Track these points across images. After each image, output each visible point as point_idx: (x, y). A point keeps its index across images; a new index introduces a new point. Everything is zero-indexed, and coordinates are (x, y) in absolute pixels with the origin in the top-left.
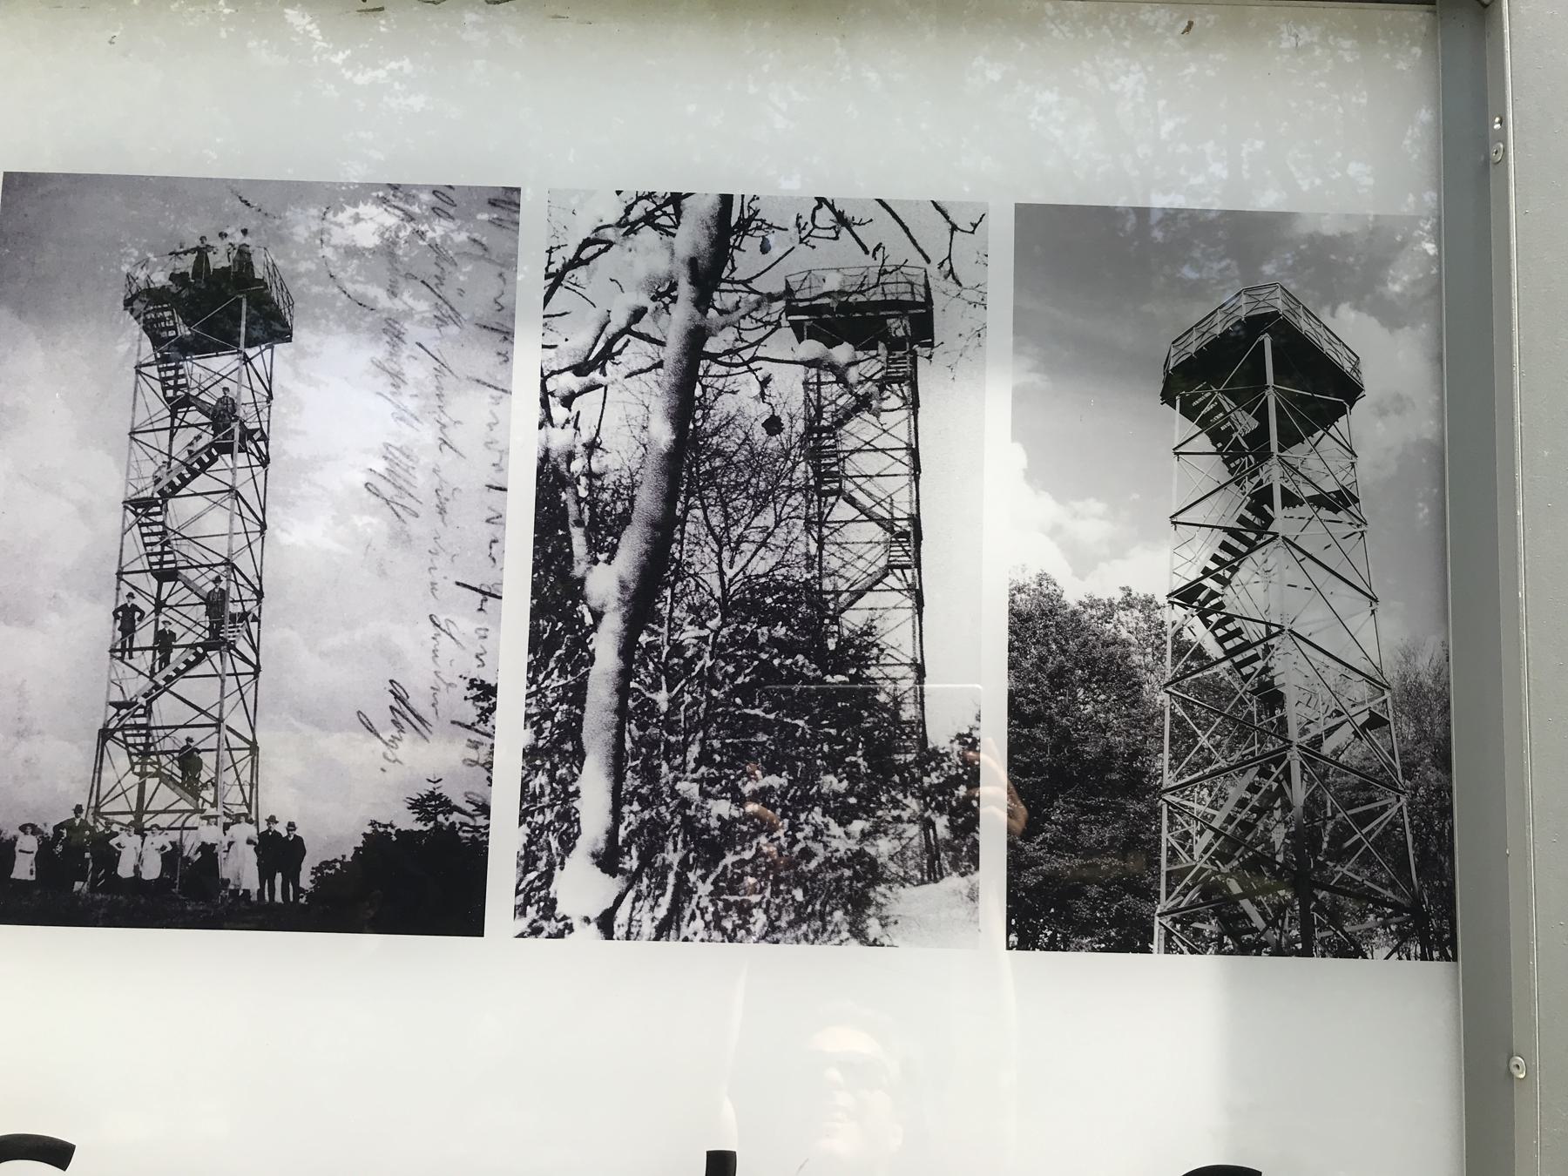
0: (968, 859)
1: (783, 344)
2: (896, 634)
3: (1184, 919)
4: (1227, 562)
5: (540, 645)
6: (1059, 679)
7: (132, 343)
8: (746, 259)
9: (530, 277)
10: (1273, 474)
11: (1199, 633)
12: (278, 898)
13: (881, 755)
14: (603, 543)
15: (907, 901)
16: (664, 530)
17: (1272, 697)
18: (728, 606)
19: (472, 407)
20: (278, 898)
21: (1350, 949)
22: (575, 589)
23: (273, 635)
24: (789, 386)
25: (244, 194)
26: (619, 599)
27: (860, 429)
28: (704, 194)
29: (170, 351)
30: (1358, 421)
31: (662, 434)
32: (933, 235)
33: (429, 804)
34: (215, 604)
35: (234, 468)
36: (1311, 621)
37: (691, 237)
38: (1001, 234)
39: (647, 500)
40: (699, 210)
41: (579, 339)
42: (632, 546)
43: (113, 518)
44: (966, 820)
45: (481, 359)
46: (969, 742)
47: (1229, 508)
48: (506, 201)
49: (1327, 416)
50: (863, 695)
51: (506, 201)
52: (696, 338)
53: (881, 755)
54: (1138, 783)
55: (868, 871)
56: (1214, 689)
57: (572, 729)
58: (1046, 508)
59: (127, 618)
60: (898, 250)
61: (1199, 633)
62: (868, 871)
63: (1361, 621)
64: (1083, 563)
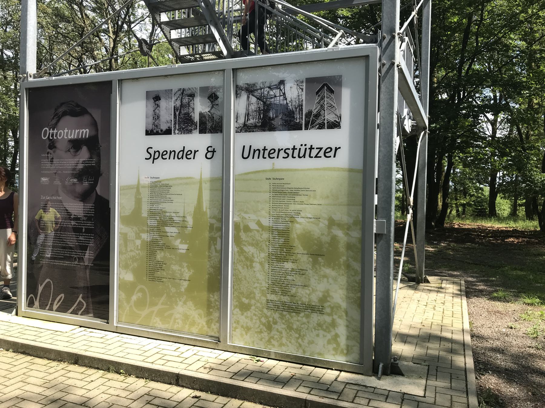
0: (197, 129)
1: (187, 97)
2: (193, 115)
3: (208, 131)
4: (211, 109)
5: (174, 117)
6: (202, 117)
7: (152, 101)
8: (185, 92)
9: (173, 95)
10: (214, 103)
11: (209, 114)
12: (94, 212)
13: (192, 123)
14: (177, 110)
15: (193, 131)
16: (180, 110)
17: (213, 118)
18: (184, 114)
19: (170, 103)
20: (94, 212)
21: (217, 133)
22: (176, 114)
23: (161, 118)
24: (187, 100)
25: (158, 91)
26: (352, 302)
27: (191, 102)
28: (182, 88)
29: (155, 101)
30: (219, 99)
31: (180, 104)
32: (195, 89)
33: (169, 127)
34: (158, 116)
35: (158, 108)
36: (216, 113)
37: (182, 91)
38: (199, 88)
39: (179, 108)
40: (182, 89)
41: (176, 98)
42: (179, 111)
43: (153, 111)
44: (197, 126)
45: (170, 100)
46: (197, 122)
47: (211, 106)
48: (172, 90)
49: (217, 99)
50: (191, 119)
51: (172, 90)
52: (182, 97)
53: (192, 123)
54: (206, 123)
55: (192, 130)
56: (210, 117)
57: (176, 122)
58: (201, 106)
59: (153, 117)
60: (193, 91)
61: (209, 114)
62: (192, 130)
63: (218, 112)
64: (203, 110)
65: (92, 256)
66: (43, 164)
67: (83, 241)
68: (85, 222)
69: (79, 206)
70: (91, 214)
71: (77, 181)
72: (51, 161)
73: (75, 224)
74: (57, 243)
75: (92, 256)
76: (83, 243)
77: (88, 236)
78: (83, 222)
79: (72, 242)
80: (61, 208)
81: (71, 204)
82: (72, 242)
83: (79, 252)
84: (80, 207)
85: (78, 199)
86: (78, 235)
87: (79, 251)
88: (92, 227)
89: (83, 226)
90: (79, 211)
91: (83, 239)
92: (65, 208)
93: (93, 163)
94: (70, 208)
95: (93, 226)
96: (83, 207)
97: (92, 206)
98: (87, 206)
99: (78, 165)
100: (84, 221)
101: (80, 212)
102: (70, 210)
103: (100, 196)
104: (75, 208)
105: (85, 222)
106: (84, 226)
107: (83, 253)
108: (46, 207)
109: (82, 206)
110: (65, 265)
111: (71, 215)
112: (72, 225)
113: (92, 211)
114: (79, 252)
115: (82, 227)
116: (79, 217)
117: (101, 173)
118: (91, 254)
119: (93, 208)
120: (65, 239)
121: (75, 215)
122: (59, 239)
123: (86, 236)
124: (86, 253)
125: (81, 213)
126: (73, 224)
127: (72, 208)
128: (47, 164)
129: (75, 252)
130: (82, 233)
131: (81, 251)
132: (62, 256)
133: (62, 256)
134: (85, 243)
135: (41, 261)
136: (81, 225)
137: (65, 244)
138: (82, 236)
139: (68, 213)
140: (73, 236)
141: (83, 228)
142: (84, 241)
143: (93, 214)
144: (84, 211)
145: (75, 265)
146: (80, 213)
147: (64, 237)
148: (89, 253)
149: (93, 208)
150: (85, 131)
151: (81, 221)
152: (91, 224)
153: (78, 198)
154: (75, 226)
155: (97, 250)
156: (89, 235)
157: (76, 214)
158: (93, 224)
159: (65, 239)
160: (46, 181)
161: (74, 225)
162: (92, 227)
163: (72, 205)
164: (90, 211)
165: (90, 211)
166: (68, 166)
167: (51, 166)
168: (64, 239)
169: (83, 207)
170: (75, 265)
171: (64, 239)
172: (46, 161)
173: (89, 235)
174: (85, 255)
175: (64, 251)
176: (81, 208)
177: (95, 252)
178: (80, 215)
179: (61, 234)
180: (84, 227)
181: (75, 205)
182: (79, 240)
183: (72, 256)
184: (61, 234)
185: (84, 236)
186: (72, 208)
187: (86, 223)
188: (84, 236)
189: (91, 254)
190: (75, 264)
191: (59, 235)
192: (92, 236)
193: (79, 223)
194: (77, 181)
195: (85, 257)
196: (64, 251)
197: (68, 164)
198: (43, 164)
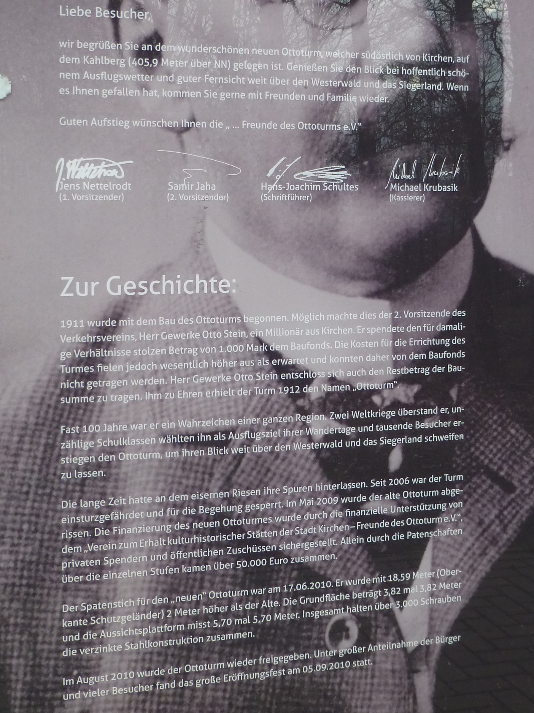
12: (461, 354)
20: (461, 354)
65: (451, 592)
66: (67, 68)
67: (389, 518)
68: (404, 412)
69: (367, 323)
70: (444, 362)
71: (348, 181)
72: (139, 54)
73: (335, 428)
74: (201, 561)
75: (451, 592)
76: (391, 531)
77: (427, 487)
78: (389, 414)
79: (314, 537)
80: (231, 348)
81: (241, 675)
82: (314, 537)
83: (364, 588)
84: (372, 331)
85: (360, 287)
86: (355, 492)
87: (366, 580)
88: (454, 437)
89: (392, 435)
90: (364, 352)
91: (396, 510)
92: (260, 341)
93: (455, 80)
94: (299, 340)
95: (458, 431)
96: (390, 329)
97: (453, 320)
98: (419, 322)
99: (355, 84)
100: (396, 405)
101: (372, 358)
102: (301, 354)
103: (498, 263)
104: (331, 339)
105: (404, 412)
106: (400, 434)
107: (389, 585)
108: (109, 345)
109: (383, 323)
110: (262, 676)
111: (309, 381)
112: (310, 439)
113: (454, 348)
114: (364, 588)
115: (385, 441)
116: (360, 386)
117: (506, 134)
118: (449, 579)
119: (458, 327)
120: (264, 527)
121: (333, 381)
122: (213, 532)
123: (413, 487)
124: (409, 584)
125: (379, 365)
126: (318, 432)
127: (313, 339)
128: (111, 69)
129: (335, 590)
130: (385, 473)
131: (378, 579)
132: (242, 628)
133: (242, 628)
134: (403, 530)
135: (74, 688)
136: (375, 435)
137: (267, 555)
138: (383, 491)
139: (280, 369)
140: (321, 501)
141: (389, 448)
142: (403, 516)
143: (455, 362)
144: (396, 351)
145: (334, 666)
146: (368, 366)
147: (255, 514)
148: (434, 580)
149: (458, 327)
150: (186, 93)
151: (375, 408)
152: (444, 417)
153: (353, 277)
154: (339, 444)
155: (484, 553)
156: (434, 479)
157: (339, 374)
158: (456, 417)
159: (264, 527)
160: (104, 179)
161: (327, 438)
162: (454, 437)
163: (313, 325)
164: (440, 349)
165: (440, 349)
166: (275, 89)
167: (143, 86)
168: (256, 527)
169: (390, 329)
170: (334, 666)
171: (256, 527)
172: (106, 53)
173: (434, 479)
174: (402, 597)
175: (260, 598)
176: (377, 337)
177: (472, 569)
178: (370, 379)
179: (230, 501)
180: (394, 442)
181: (333, 324)
182: (364, 519)
183: (316, 615)
184: (230, 501)
185: (399, 489)
186: (313, 339)
187: (412, 419)
188: (399, 489)
189: (449, 579)
190: (336, 658)
191: (213, 511)
192: (451, 485)
193: (367, 422)
194: (348, 181)
195: (408, 603)
196: (260, 598)
197: (281, 75)
198: (67, 68)
